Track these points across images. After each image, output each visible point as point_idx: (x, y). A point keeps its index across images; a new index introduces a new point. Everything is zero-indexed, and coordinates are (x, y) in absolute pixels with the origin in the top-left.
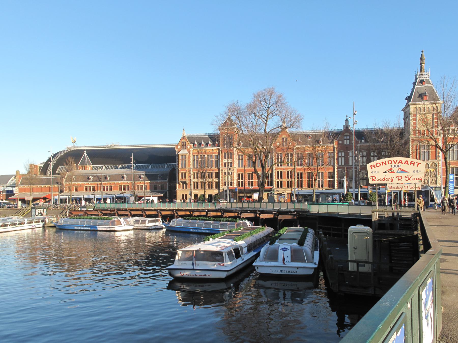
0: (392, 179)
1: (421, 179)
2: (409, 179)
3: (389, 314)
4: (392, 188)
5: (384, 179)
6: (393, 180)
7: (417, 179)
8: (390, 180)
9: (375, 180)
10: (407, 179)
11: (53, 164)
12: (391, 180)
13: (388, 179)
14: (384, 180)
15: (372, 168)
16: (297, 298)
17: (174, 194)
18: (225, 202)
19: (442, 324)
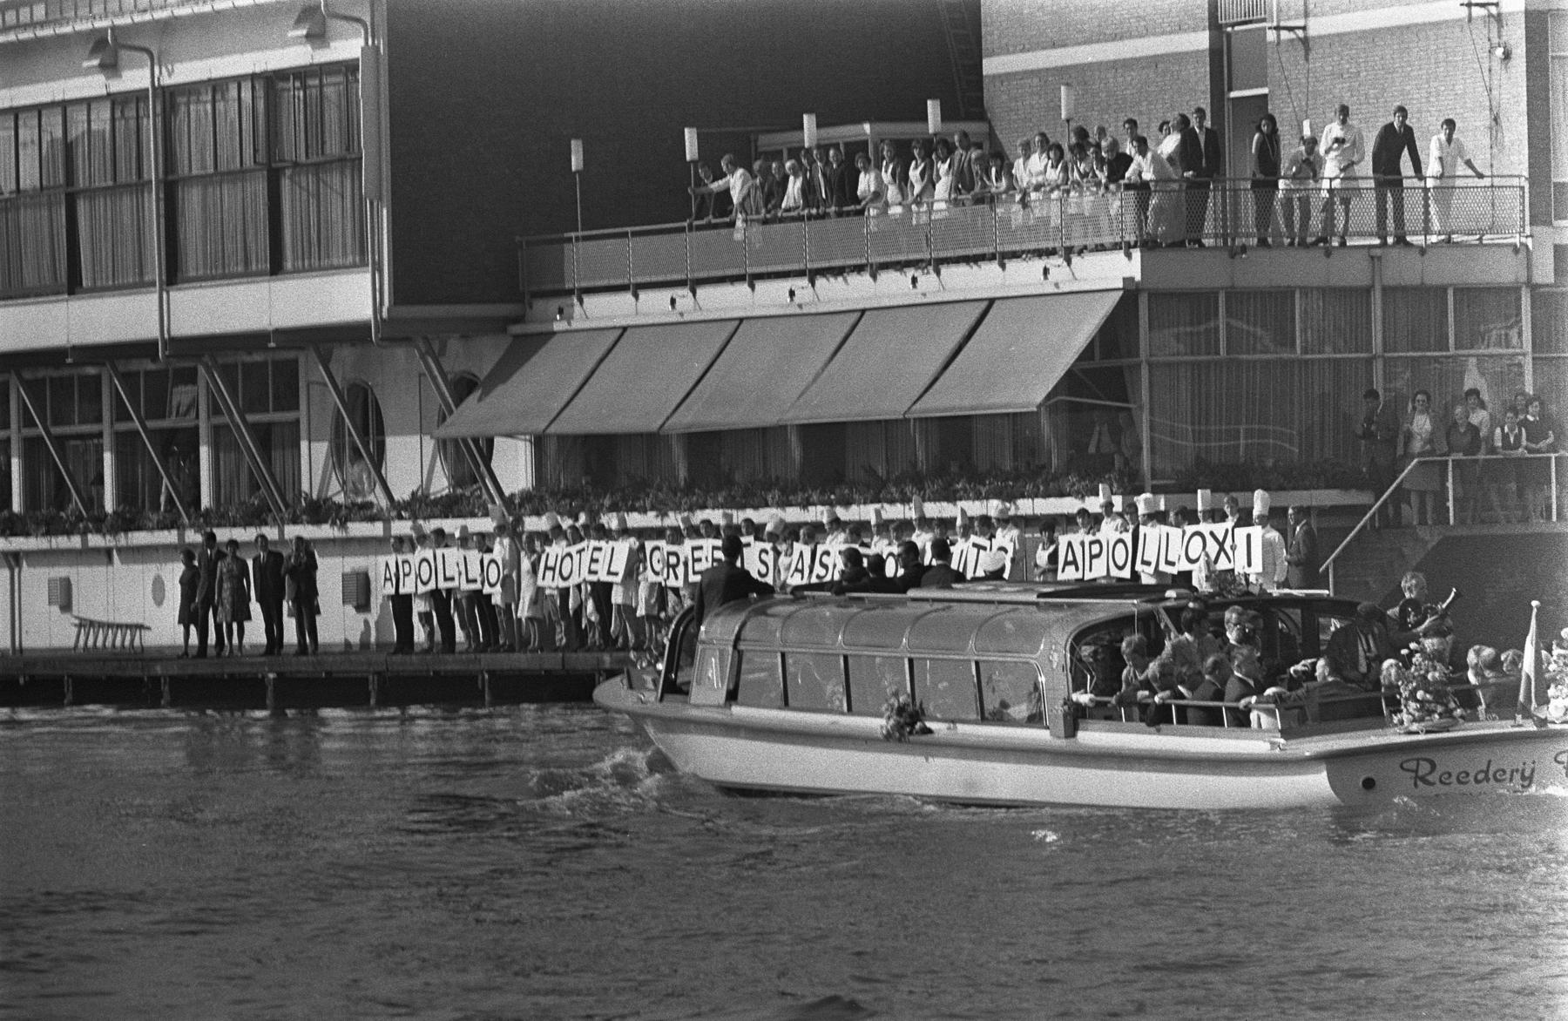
5: (1487, 772)
6: (1531, 779)
8: (1517, 776)
9: (1430, 778)
12: (1523, 778)
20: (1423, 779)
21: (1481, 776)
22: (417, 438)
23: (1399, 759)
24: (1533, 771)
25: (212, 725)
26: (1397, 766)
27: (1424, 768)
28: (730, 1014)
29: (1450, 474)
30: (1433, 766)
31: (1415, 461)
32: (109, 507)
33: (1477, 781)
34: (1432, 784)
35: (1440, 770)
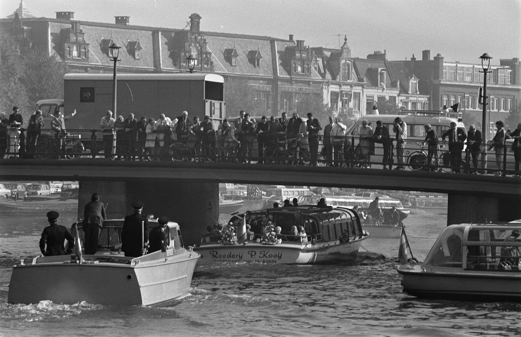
0: (241, 256)
1: (280, 256)
2: (264, 255)
3: (129, 66)
4: (217, 256)
5: (230, 255)
6: (242, 257)
7: (275, 256)
8: (238, 257)
9: (217, 256)
10: (262, 256)
11: (23, 306)
12: (239, 257)
13: (236, 256)
14: (230, 257)
15: (252, 257)
16: (471, 154)
17: (181, 236)
18: (178, 70)
19: (25, 235)
20: (215, 256)
21: (229, 256)
22: (383, 154)
23: (208, 251)
24: (281, 255)
25: (510, 250)
26: (247, 252)
27: (215, 254)
28: (33, 236)
29: (113, 220)
30: (217, 253)
31: (133, 117)
32: (506, 176)
33: (228, 257)
34: (217, 257)
35: (218, 254)
